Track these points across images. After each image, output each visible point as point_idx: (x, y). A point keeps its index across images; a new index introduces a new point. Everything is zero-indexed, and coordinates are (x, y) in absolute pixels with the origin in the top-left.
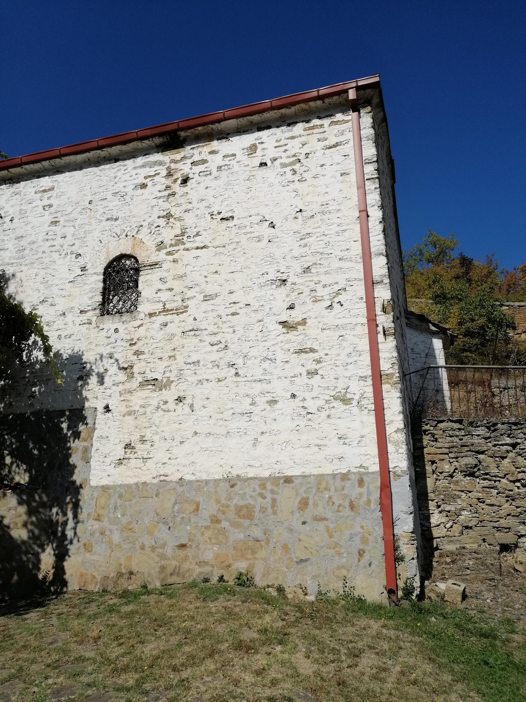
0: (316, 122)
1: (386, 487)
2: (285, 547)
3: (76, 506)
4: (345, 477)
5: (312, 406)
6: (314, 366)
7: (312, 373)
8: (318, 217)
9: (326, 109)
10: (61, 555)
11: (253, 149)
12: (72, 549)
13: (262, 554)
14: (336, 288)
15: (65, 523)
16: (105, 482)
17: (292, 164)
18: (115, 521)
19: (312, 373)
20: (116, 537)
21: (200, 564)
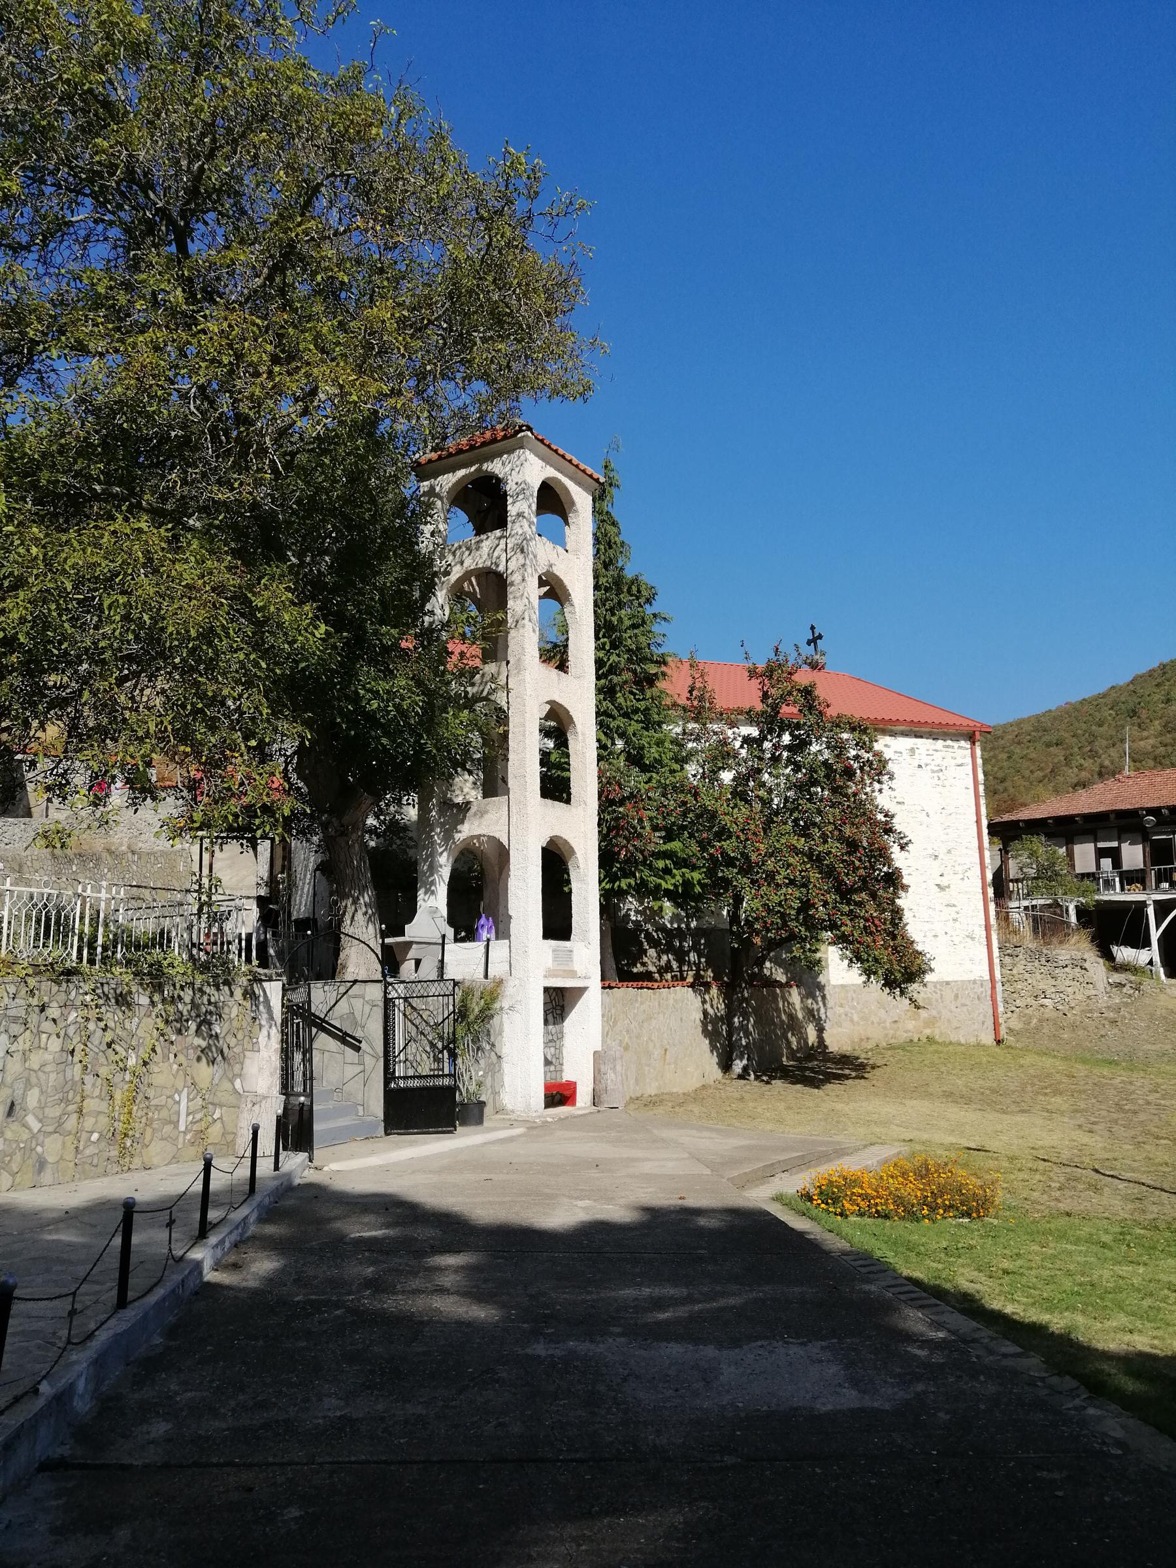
0: (949, 742)
1: (993, 988)
2: (949, 1020)
3: (824, 997)
4: (974, 982)
5: (957, 940)
6: (955, 916)
7: (955, 920)
8: (954, 816)
9: (955, 735)
10: (820, 1030)
11: (912, 751)
12: (827, 1026)
13: (937, 1025)
14: (966, 867)
15: (818, 1010)
16: (840, 982)
17: (937, 771)
18: (854, 1008)
19: (955, 920)
20: (856, 1018)
21: (906, 1032)
